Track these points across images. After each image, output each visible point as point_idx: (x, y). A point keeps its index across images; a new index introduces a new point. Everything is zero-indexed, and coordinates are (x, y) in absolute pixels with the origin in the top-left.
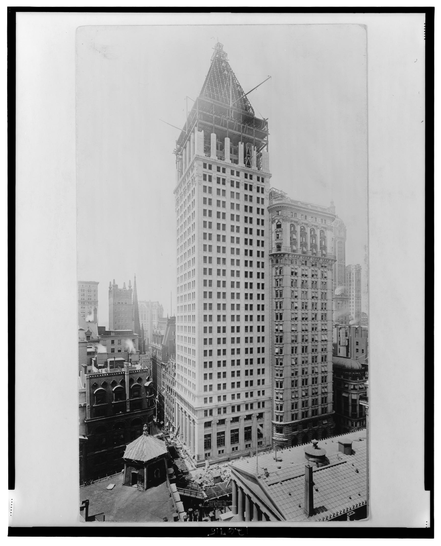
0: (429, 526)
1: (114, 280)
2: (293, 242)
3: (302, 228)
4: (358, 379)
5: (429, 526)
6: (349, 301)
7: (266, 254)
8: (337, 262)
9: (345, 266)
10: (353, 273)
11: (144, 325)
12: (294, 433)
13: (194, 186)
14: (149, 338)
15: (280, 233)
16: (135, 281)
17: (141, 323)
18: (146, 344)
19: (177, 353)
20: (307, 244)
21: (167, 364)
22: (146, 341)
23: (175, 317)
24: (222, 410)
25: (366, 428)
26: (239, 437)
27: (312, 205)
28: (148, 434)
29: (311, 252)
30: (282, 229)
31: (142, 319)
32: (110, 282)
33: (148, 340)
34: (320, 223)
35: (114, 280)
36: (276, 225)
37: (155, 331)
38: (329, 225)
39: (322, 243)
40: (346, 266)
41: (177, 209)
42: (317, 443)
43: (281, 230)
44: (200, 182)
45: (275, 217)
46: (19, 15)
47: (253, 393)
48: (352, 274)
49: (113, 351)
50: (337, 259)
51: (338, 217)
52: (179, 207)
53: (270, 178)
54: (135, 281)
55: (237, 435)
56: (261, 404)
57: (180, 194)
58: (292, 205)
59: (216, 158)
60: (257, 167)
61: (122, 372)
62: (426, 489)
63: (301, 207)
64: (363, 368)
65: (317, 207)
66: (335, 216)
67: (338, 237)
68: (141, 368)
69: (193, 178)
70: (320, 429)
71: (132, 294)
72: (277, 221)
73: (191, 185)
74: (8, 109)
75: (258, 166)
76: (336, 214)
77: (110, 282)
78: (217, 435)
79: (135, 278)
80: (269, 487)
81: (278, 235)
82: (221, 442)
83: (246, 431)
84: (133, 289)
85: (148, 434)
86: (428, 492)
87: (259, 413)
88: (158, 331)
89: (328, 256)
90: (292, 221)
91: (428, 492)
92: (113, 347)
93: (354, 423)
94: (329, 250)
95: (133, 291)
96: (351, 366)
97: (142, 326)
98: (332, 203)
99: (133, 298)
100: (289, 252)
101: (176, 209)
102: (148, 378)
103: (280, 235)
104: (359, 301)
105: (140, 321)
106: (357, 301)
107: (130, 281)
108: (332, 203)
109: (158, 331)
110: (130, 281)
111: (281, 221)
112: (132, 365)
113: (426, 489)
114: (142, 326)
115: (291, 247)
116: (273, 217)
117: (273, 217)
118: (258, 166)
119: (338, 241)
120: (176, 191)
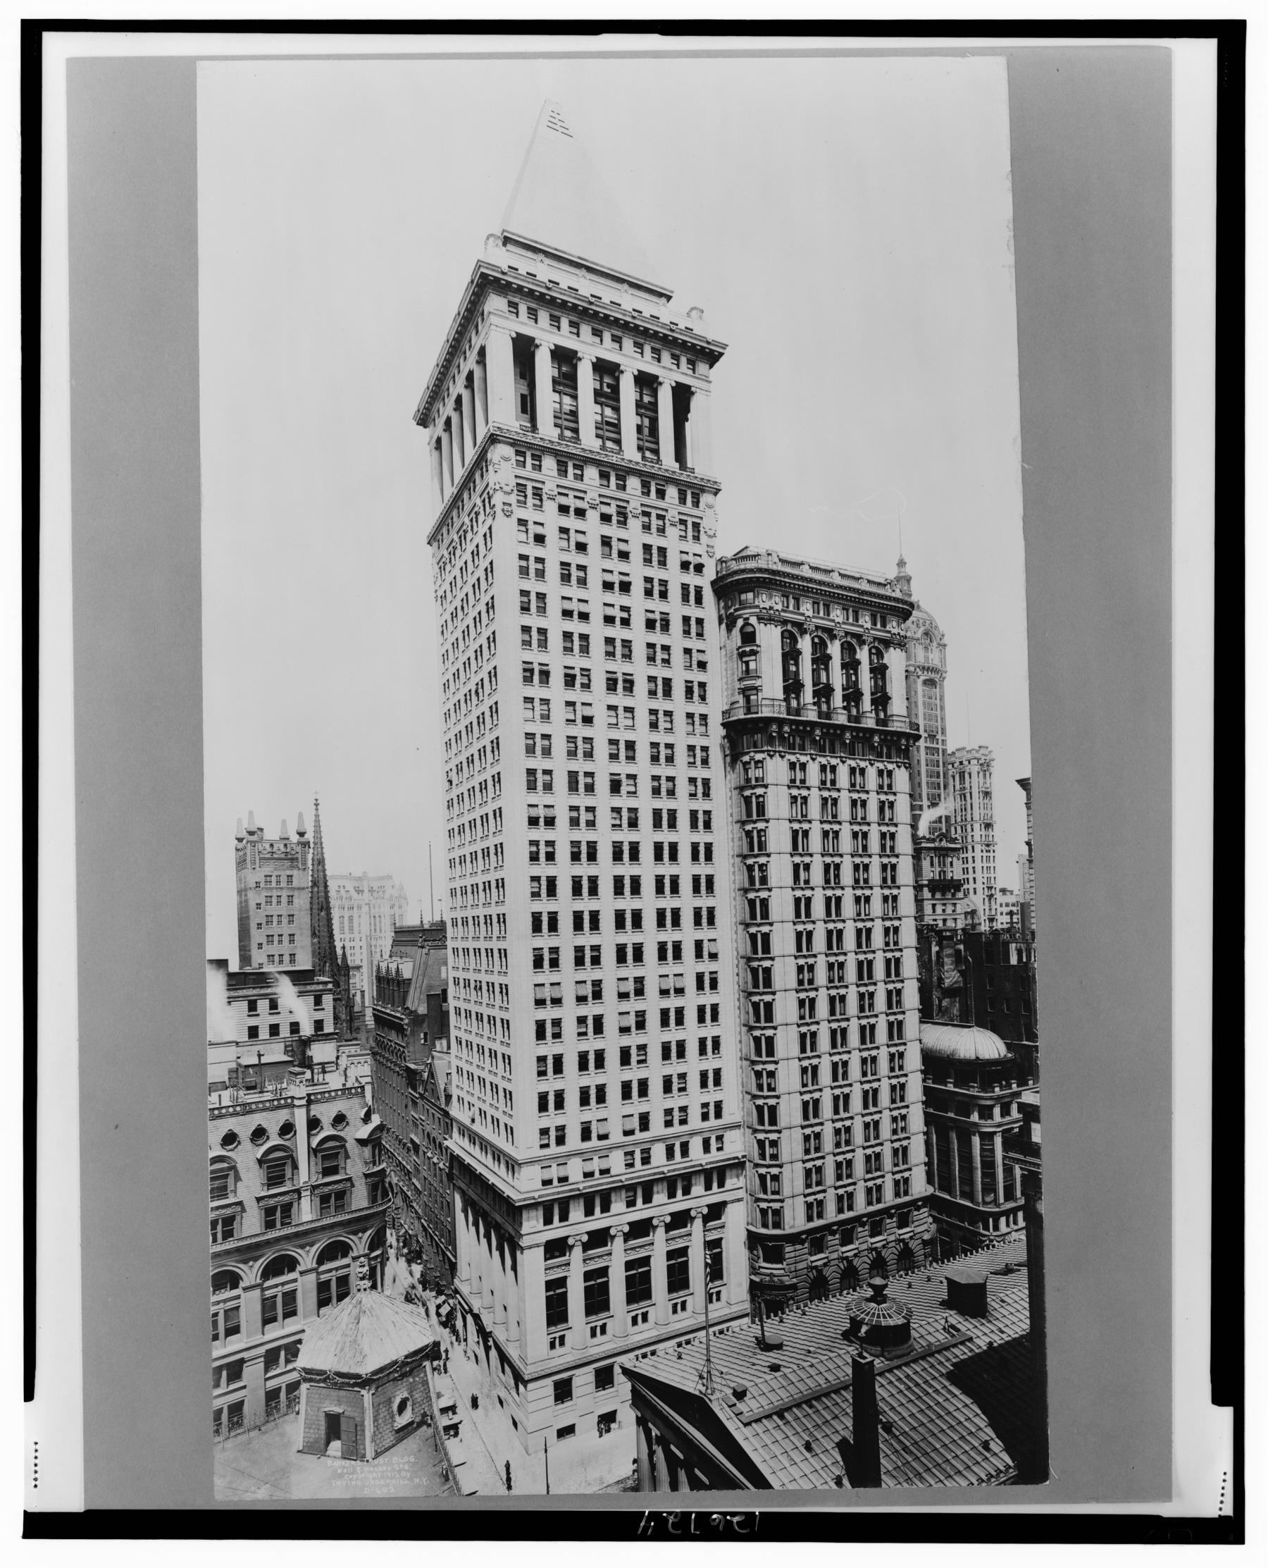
0: (1228, 1510)
1: (251, 813)
2: (792, 687)
3: (816, 640)
4: (997, 1089)
5: (1228, 1510)
6: (962, 856)
7: (715, 721)
8: (922, 740)
9: (944, 751)
10: (970, 774)
11: (348, 952)
12: (844, 1249)
13: (489, 521)
14: (366, 988)
15: (753, 658)
16: (317, 816)
17: (338, 945)
18: (357, 1009)
19: (453, 1033)
20: (803, 686)
21: (422, 1067)
22: (358, 999)
23: (443, 923)
24: (596, 1200)
25: (339, 1438)
26: (624, 1291)
27: (842, 572)
28: (625, 1234)
29: (815, 708)
30: (758, 646)
31: (342, 929)
32: (239, 820)
33: (363, 996)
34: (869, 625)
35: (251, 813)
36: (739, 634)
37: (383, 966)
38: (894, 631)
39: (819, 677)
40: (949, 752)
41: (440, 593)
42: (886, 1286)
43: (755, 648)
44: (506, 508)
45: (736, 610)
46: (52, 42)
47: (690, 1144)
48: (967, 776)
49: (253, 1032)
50: (922, 732)
51: (918, 606)
52: (447, 586)
53: (716, 494)
54: (317, 816)
55: (605, 1288)
56: (716, 1175)
57: (446, 546)
58: (784, 573)
59: (637, 457)
60: (677, 460)
61: (285, 1099)
62: (1218, 1399)
63: (811, 580)
64: (1010, 1055)
65: (828, 572)
66: (912, 605)
67: (924, 668)
68: (344, 1085)
69: (485, 495)
70: (893, 1244)
71: (310, 856)
72: (740, 622)
73: (481, 518)
74: (22, 314)
75: (680, 455)
76: (914, 599)
77: (239, 820)
78: (586, 1280)
79: (317, 805)
80: (747, 1431)
81: (747, 663)
82: (597, 1300)
83: (552, 1293)
84: (312, 840)
85: (625, 1234)
86: (1227, 1412)
87: (629, 1223)
88: (393, 967)
89: (764, 709)
90: (785, 622)
91: (1227, 1412)
92: (253, 1022)
93: (991, 1220)
94: (897, 706)
95: (312, 845)
96: (977, 1058)
97: (344, 953)
98: (901, 564)
99: (311, 867)
100: (781, 716)
101: (436, 591)
102: (365, 1115)
103: (752, 666)
104: (991, 854)
105: (335, 938)
106: (985, 854)
107: (301, 815)
108: (901, 564)
109: (393, 967)
110: (301, 815)
111: (753, 620)
112: (316, 1077)
113: (1218, 1399)
114: (344, 953)
115: (787, 700)
116: (732, 611)
117: (732, 611)
118: (680, 455)
119: (922, 678)
120: (434, 538)
